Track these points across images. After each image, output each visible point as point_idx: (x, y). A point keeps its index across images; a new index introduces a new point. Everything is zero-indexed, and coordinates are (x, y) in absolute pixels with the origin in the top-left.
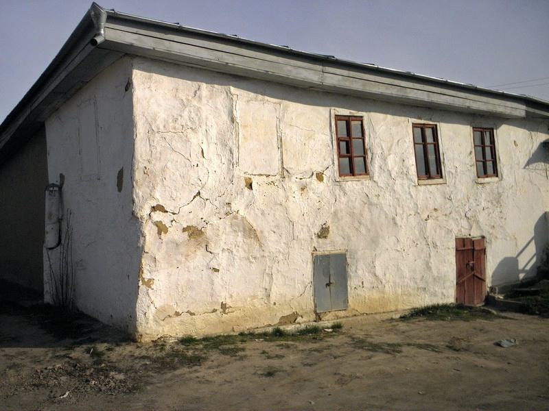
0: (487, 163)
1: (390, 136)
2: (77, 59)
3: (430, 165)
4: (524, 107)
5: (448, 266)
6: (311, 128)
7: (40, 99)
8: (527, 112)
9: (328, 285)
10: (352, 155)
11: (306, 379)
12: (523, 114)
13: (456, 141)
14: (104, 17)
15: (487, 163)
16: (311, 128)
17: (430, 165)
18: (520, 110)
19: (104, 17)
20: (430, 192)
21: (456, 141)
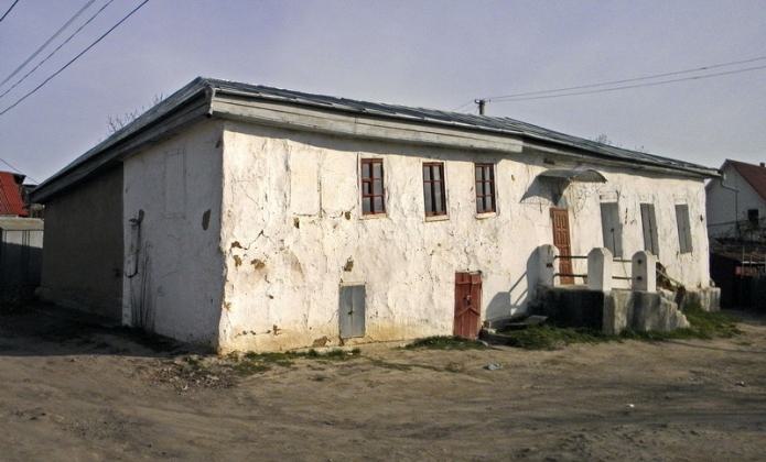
0: (486, 199)
3: (436, 203)
4: (521, 143)
10: (373, 198)
15: (486, 199)
17: (436, 203)
18: (517, 146)
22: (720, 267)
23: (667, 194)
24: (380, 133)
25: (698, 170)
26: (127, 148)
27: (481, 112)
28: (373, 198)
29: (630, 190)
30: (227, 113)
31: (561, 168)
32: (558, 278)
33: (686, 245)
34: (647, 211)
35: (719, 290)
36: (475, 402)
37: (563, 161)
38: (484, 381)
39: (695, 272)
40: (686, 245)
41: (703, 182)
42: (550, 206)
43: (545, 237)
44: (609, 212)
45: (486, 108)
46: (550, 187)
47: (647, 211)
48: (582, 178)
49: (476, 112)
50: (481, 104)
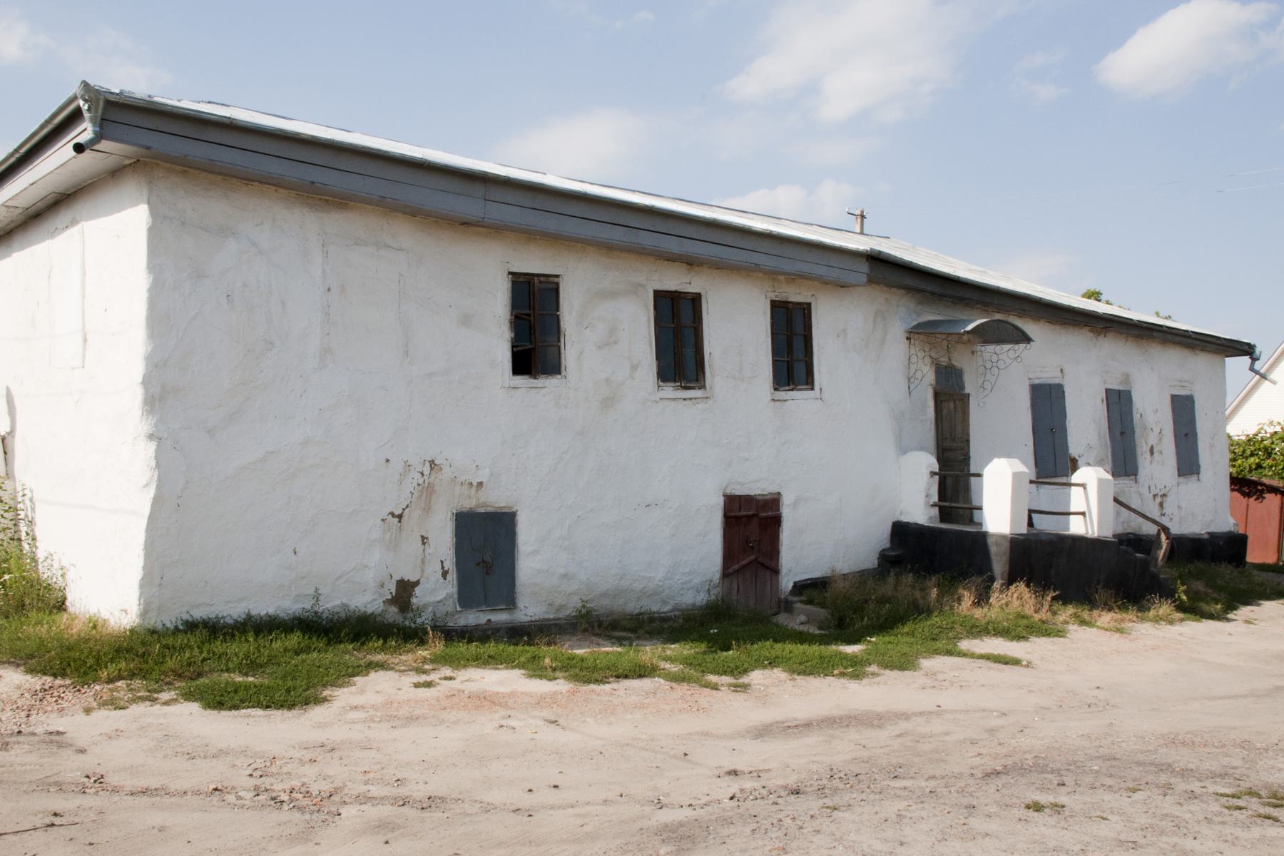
0: (793, 362)
1: (607, 322)
3: (679, 351)
10: (534, 350)
13: (736, 328)
17: (679, 351)
21: (736, 328)
28: (534, 350)
29: (1047, 354)
47: (1119, 404)
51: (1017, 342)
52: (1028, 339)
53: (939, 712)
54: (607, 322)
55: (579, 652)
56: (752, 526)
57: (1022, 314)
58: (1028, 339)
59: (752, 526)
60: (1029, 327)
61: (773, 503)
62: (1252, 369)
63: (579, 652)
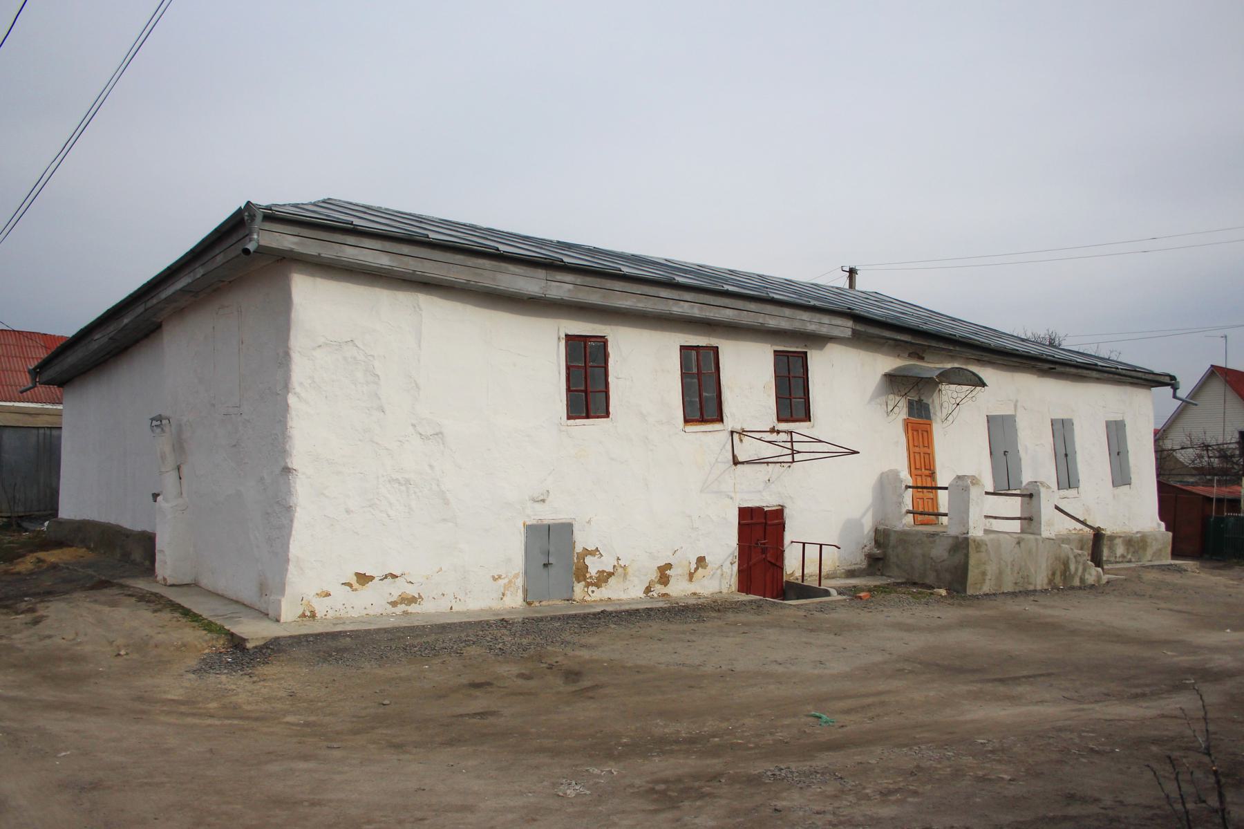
0: (793, 398)
1: (644, 366)
2: (219, 258)
3: (703, 400)
4: (850, 323)
5: (723, 545)
6: (532, 353)
7: (163, 295)
8: (854, 331)
9: (546, 565)
10: (587, 391)
11: (184, 469)
12: (848, 333)
13: (747, 373)
14: (259, 218)
15: (793, 398)
16: (532, 353)
17: (703, 400)
18: (845, 327)
19: (259, 218)
20: (711, 438)
21: (747, 373)
22: (1172, 500)
23: (1090, 405)
24: (595, 298)
25: (1140, 375)
26: (155, 301)
27: (852, 285)
28: (587, 391)
29: (1003, 389)
30: (291, 251)
31: (932, 366)
32: (943, 509)
33: (1121, 477)
34: (1062, 430)
35: (1170, 534)
36: (186, 613)
37: (927, 353)
38: (834, 615)
39: (1137, 511)
40: (1121, 477)
41: (259, 246)
42: (905, 417)
43: (898, 461)
44: (1001, 432)
45: (859, 279)
46: (913, 394)
47: (1062, 430)
48: (949, 377)
49: (843, 282)
50: (852, 272)
51: (975, 385)
52: (984, 385)
53: (889, 692)
54: (644, 366)
55: (126, 321)
56: (761, 531)
57: (980, 362)
58: (984, 385)
59: (761, 531)
60: (985, 373)
61: (779, 514)
62: (1175, 396)
63: (126, 321)
